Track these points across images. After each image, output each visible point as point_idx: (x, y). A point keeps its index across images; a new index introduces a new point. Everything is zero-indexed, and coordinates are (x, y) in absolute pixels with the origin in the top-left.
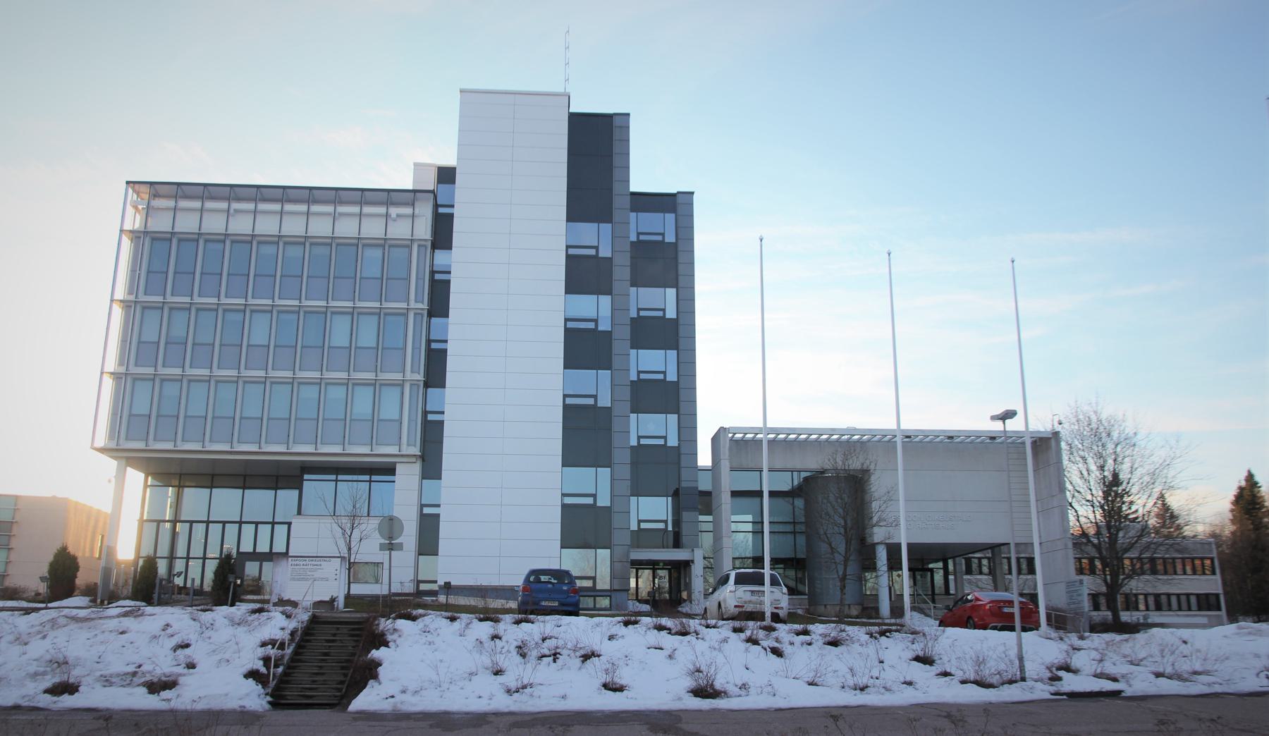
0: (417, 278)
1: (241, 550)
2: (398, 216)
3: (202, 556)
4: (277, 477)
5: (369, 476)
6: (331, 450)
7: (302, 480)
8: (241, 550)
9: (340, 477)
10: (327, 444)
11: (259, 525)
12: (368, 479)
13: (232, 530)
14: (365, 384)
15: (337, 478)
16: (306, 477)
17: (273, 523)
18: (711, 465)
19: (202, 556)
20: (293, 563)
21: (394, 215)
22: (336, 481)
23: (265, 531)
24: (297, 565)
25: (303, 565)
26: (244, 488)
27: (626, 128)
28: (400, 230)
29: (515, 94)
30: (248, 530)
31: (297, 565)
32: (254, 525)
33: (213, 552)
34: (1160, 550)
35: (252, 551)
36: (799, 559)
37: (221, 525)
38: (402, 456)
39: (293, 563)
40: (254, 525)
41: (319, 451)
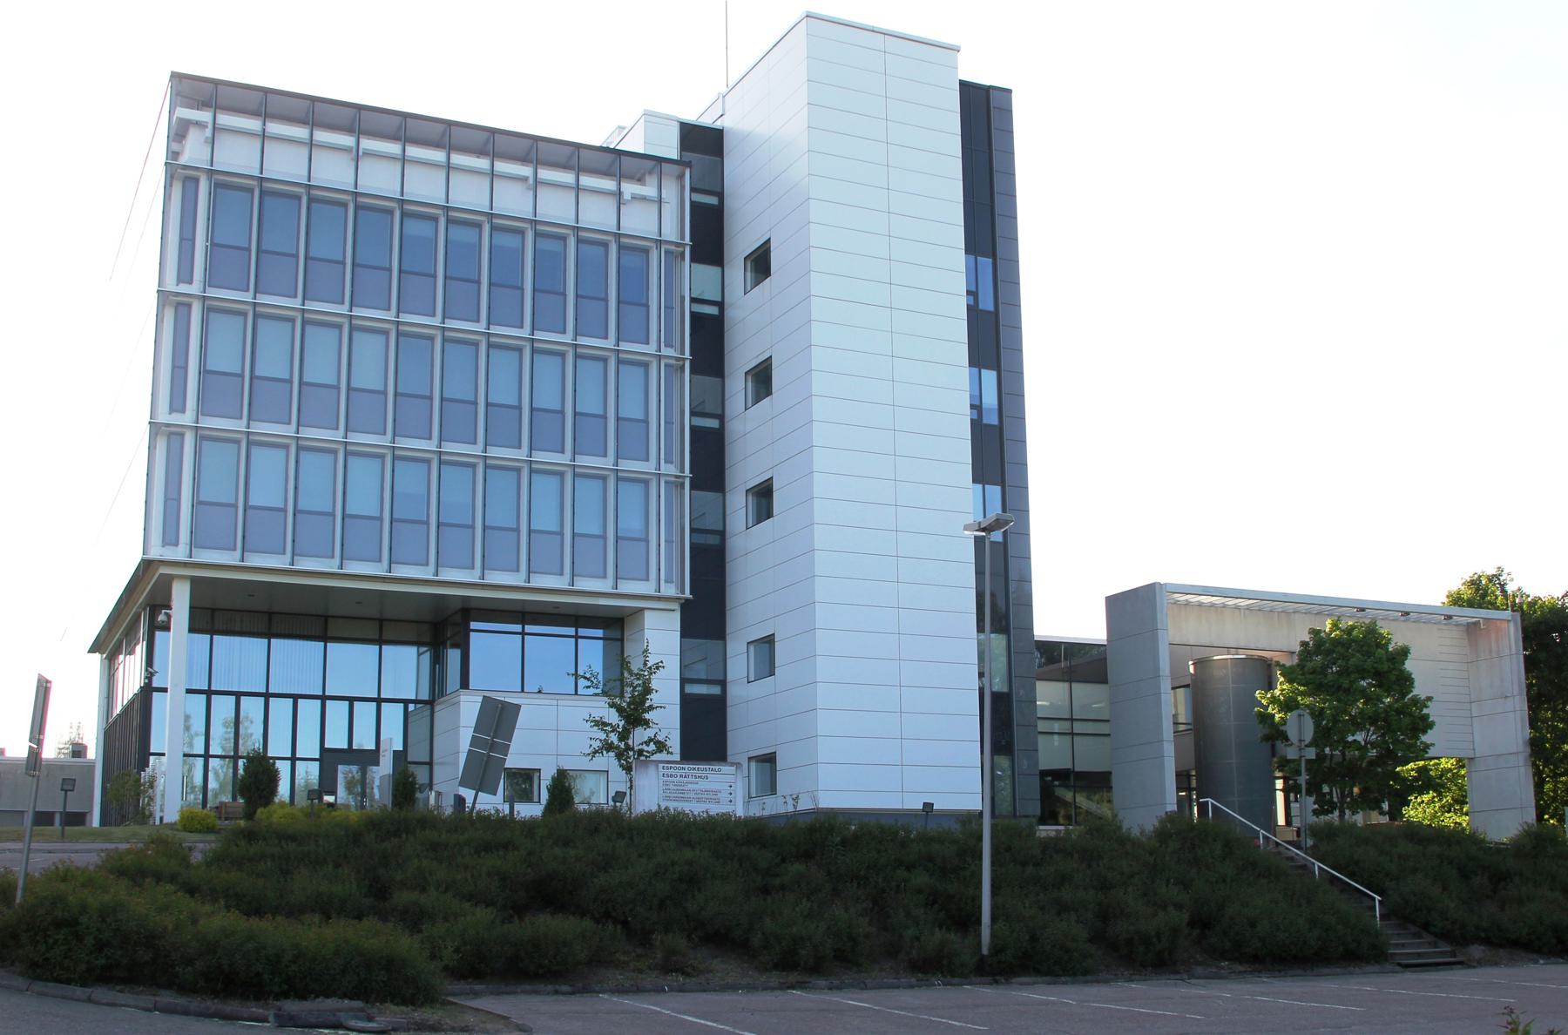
0: (193, 240)
1: (327, 745)
2: (635, 198)
3: (289, 755)
4: (213, 610)
5: (574, 629)
6: (506, 580)
7: (468, 631)
8: (327, 745)
9: (582, 632)
10: (542, 573)
11: (300, 701)
12: (520, 630)
13: (365, 712)
14: (328, 451)
15: (577, 632)
16: (474, 625)
17: (267, 696)
18: (1105, 638)
19: (289, 755)
20: (666, 771)
21: (627, 196)
22: (523, 634)
23: (365, 712)
24: (671, 776)
25: (681, 776)
26: (380, 641)
27: (1007, 112)
28: (639, 222)
29: (885, 34)
30: (337, 711)
31: (671, 776)
32: (402, 705)
33: (309, 746)
34: (67, 749)
35: (345, 746)
36: (1077, 772)
37: (233, 698)
38: (659, 599)
39: (666, 771)
40: (402, 705)
41: (532, 584)
